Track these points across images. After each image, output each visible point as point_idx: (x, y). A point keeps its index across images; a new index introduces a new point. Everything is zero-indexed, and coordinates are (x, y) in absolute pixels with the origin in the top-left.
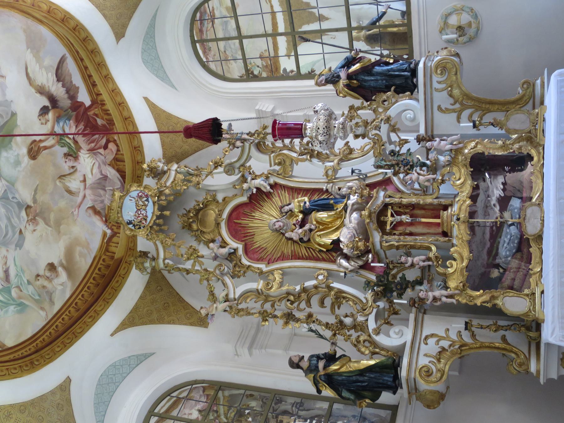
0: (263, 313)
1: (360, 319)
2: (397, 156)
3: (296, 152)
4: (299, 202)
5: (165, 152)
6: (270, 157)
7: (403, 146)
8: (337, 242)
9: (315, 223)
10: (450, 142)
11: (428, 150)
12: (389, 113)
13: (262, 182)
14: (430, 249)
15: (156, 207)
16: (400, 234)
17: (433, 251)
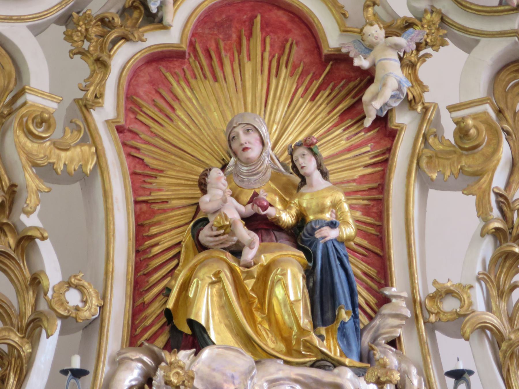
3: (508, 185)
4: (335, 205)
6: (481, 102)
9: (265, 259)
13: (392, 85)
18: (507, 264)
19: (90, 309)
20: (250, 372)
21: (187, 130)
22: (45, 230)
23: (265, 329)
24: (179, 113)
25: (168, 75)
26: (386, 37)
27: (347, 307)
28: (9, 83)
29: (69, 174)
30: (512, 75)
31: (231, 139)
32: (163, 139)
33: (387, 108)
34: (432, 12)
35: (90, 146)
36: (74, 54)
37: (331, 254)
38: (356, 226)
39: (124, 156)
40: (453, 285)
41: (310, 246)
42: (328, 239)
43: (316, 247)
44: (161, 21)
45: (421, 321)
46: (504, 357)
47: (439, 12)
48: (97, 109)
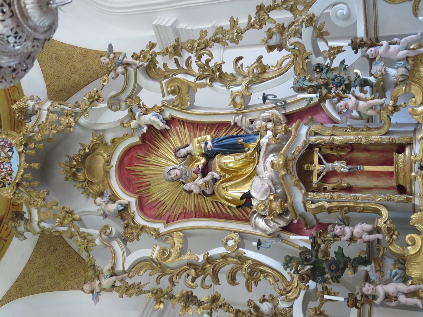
0: (156, 293)
1: (283, 305)
2: (327, 72)
3: (193, 76)
4: (199, 142)
5: (49, 85)
6: (161, 85)
7: (334, 57)
8: (247, 197)
9: (218, 170)
10: (405, 45)
11: (372, 60)
12: (311, 10)
14: (379, 212)
15: (23, 158)
16: (334, 190)
17: (384, 217)
18: (223, 77)
19: (235, 237)
20: (261, 178)
21: (169, 197)
22: (205, 253)
23: (245, 171)
24: (162, 199)
25: (147, 203)
26: (135, 120)
27: (238, 139)
28: (148, 264)
29: (184, 242)
30: (151, 72)
31: (173, 180)
32: (172, 206)
33: (163, 120)
34: (126, 101)
35: (174, 234)
36: (138, 239)
37: (217, 144)
38: (207, 134)
39: (178, 221)
40: (231, 98)
41: (214, 152)
42: (211, 146)
43: (214, 150)
44: (127, 205)
45: (244, 111)
46: (259, 80)
47: (127, 99)
48: (160, 231)
